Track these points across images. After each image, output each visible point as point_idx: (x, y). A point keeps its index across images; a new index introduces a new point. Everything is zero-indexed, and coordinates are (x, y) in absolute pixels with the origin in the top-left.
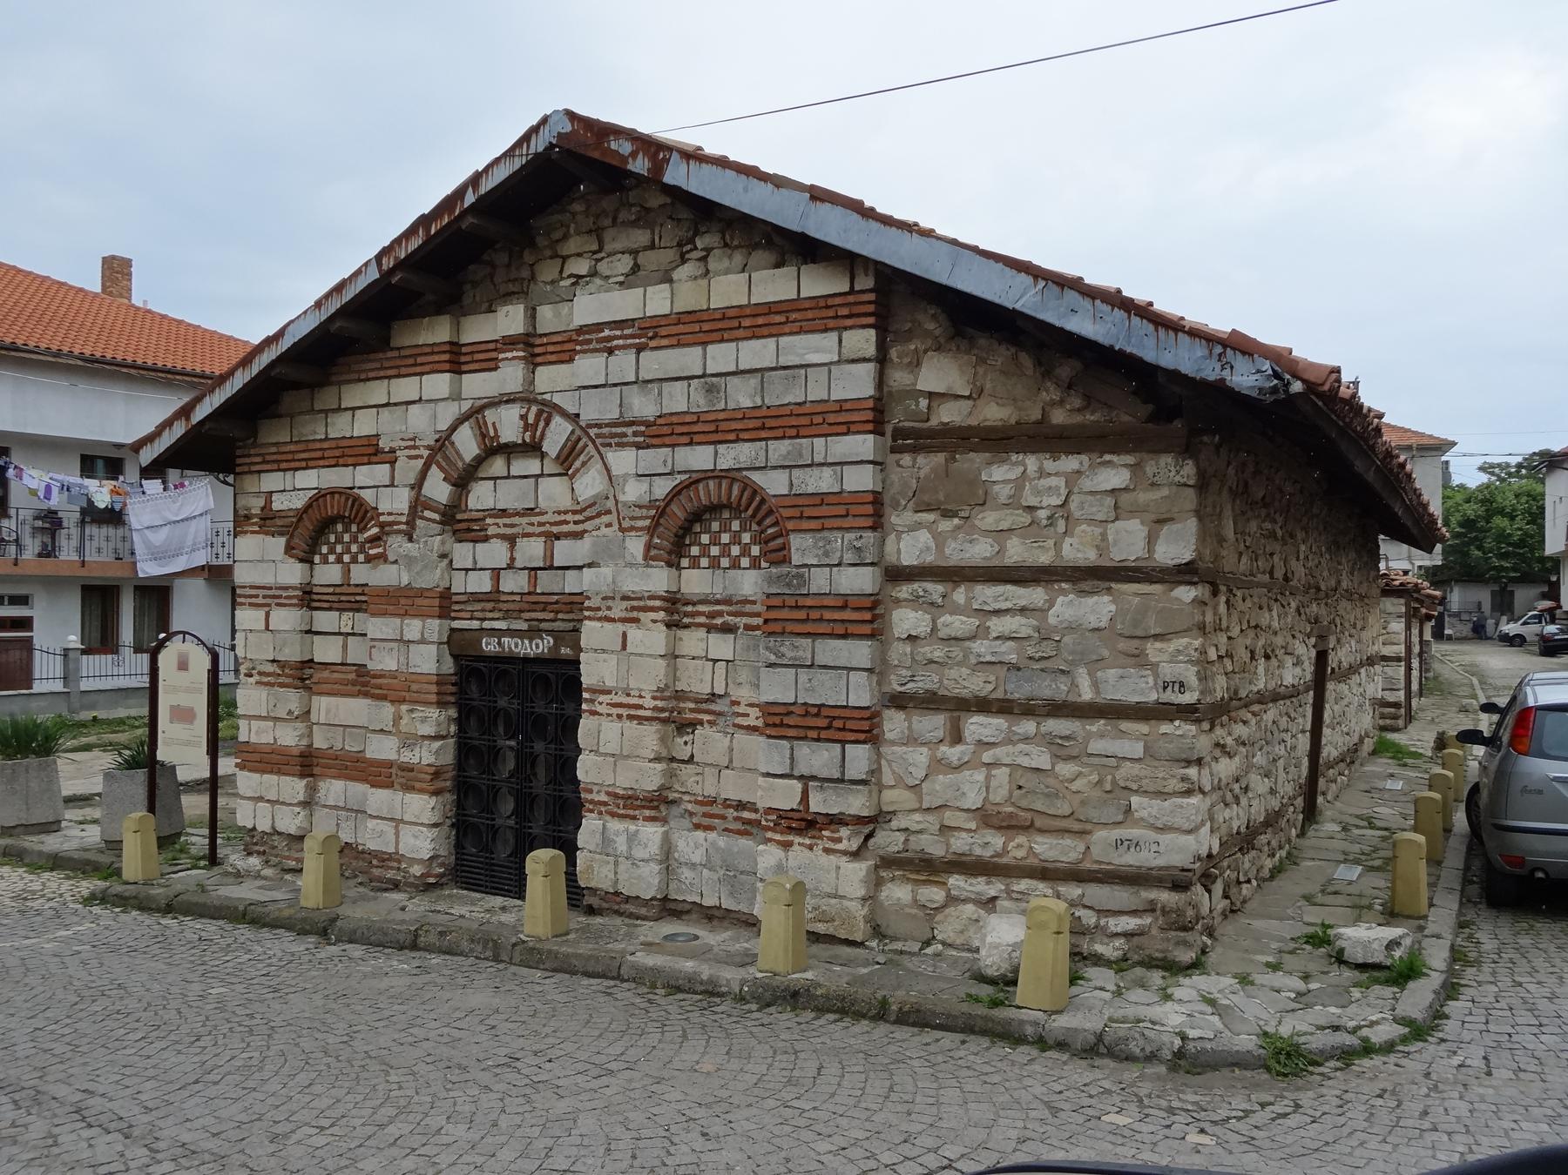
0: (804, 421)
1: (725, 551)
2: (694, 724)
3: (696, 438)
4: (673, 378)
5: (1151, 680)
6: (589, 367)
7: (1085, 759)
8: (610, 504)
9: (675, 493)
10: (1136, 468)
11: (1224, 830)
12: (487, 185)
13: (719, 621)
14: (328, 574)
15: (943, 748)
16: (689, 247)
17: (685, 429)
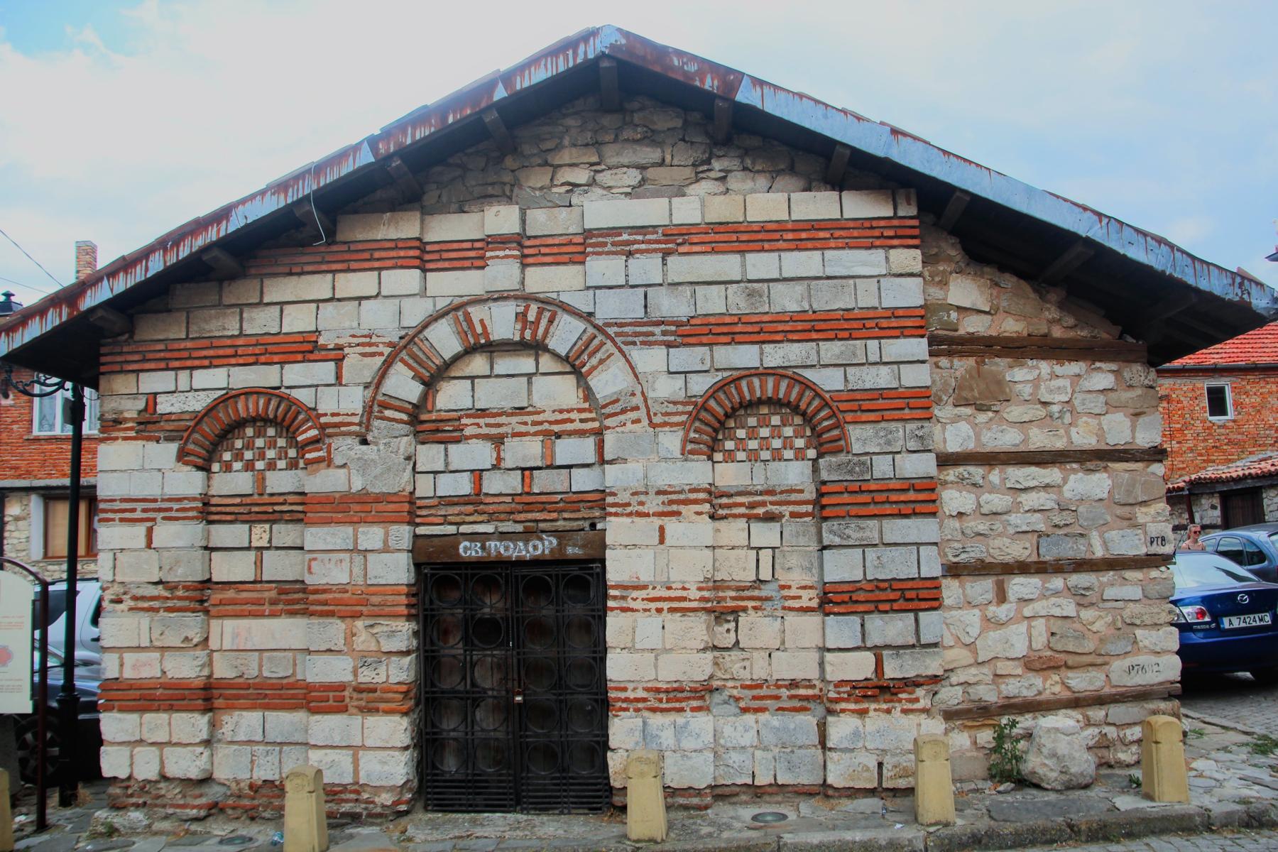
0: (855, 324)
2: (735, 611)
4: (712, 283)
5: (1142, 537)
6: (604, 268)
8: (638, 400)
12: (522, 83)
13: (760, 511)
14: (233, 482)
15: (992, 608)
16: (705, 167)
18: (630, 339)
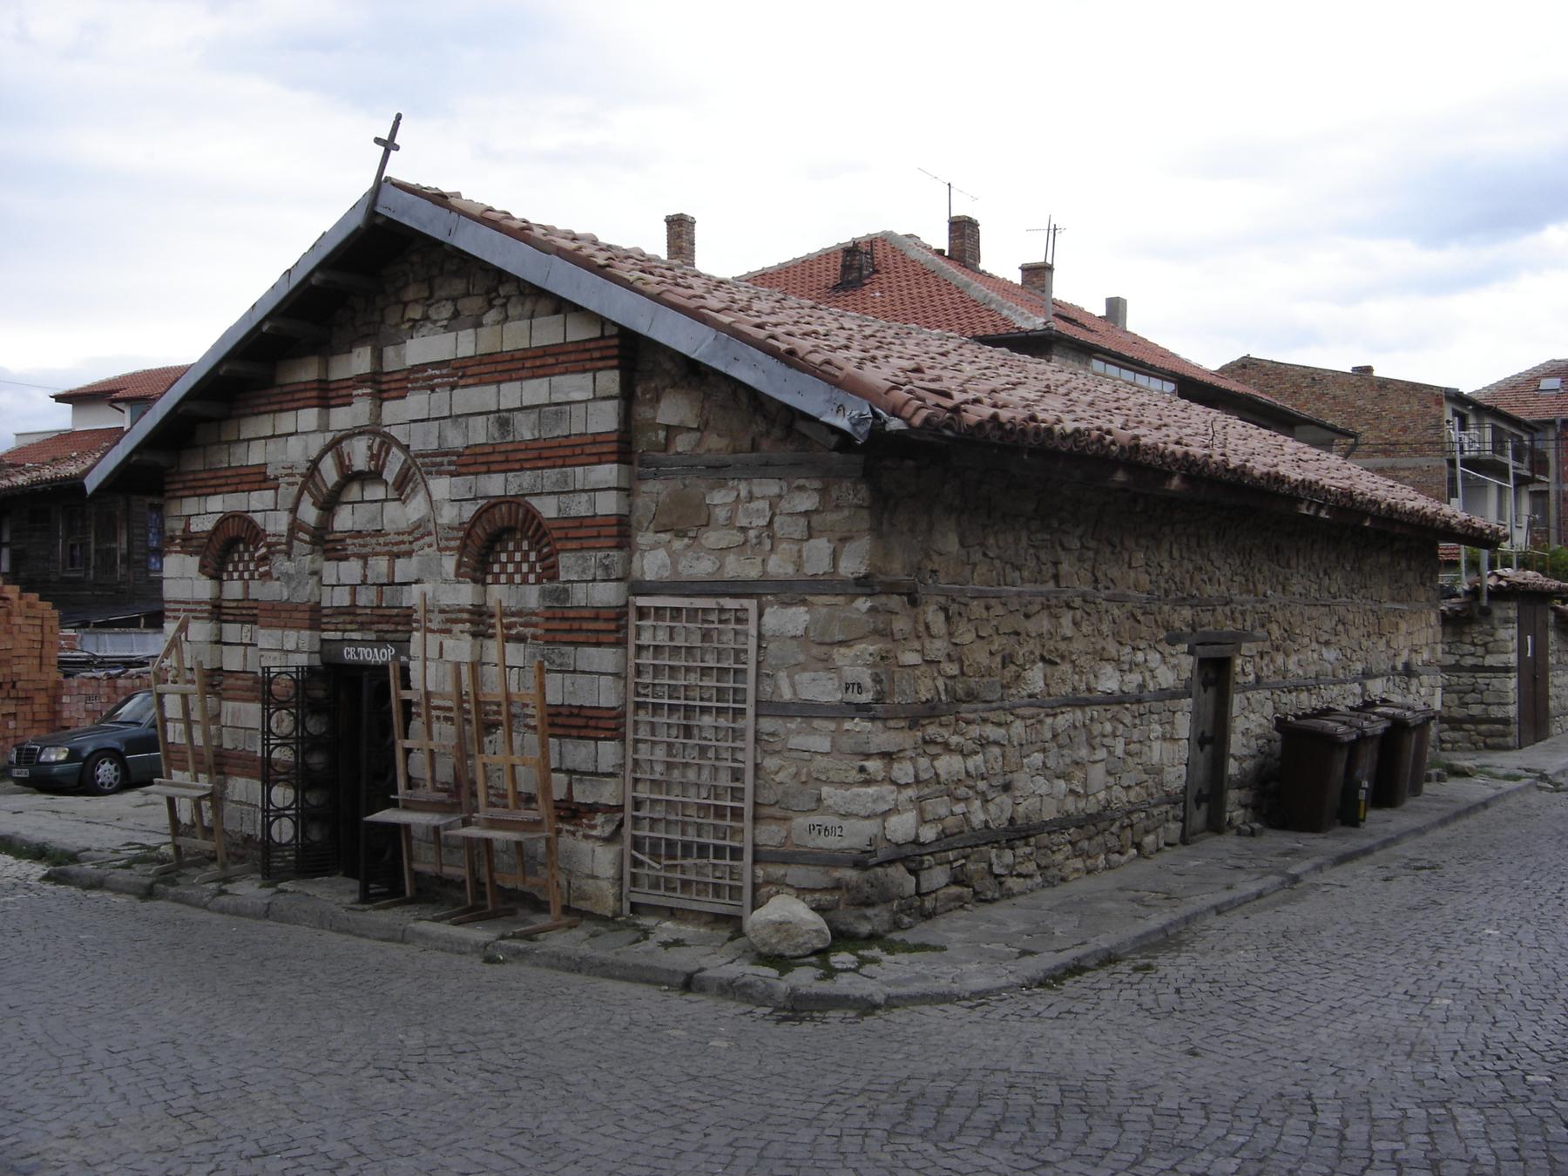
0: (568, 452)
1: (518, 570)
3: (493, 467)
6: (416, 403)
7: (787, 754)
8: (431, 526)
9: (478, 517)
10: (823, 492)
13: (514, 632)
17: (483, 459)
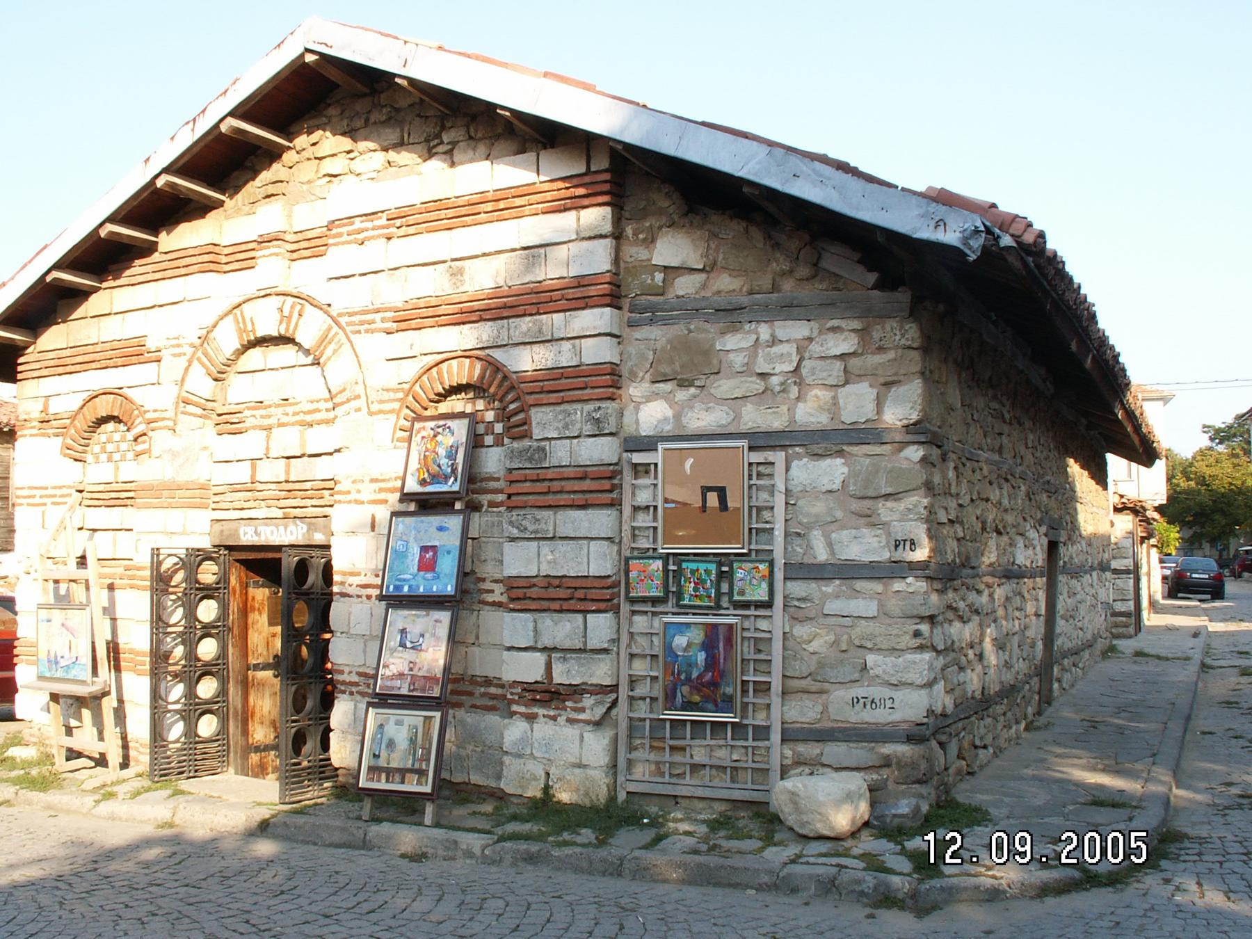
7: (821, 620)
10: (863, 333)
11: (957, 692)
16: (436, 142)
18: (357, 328)
